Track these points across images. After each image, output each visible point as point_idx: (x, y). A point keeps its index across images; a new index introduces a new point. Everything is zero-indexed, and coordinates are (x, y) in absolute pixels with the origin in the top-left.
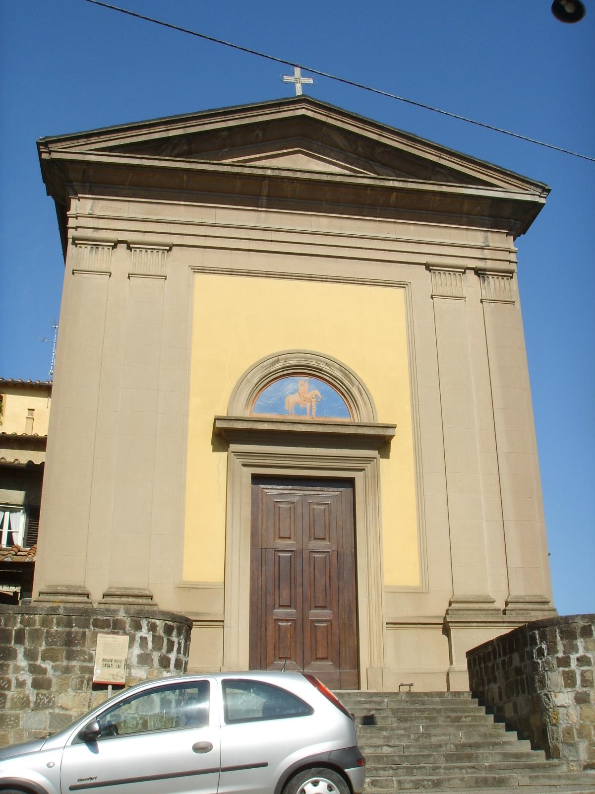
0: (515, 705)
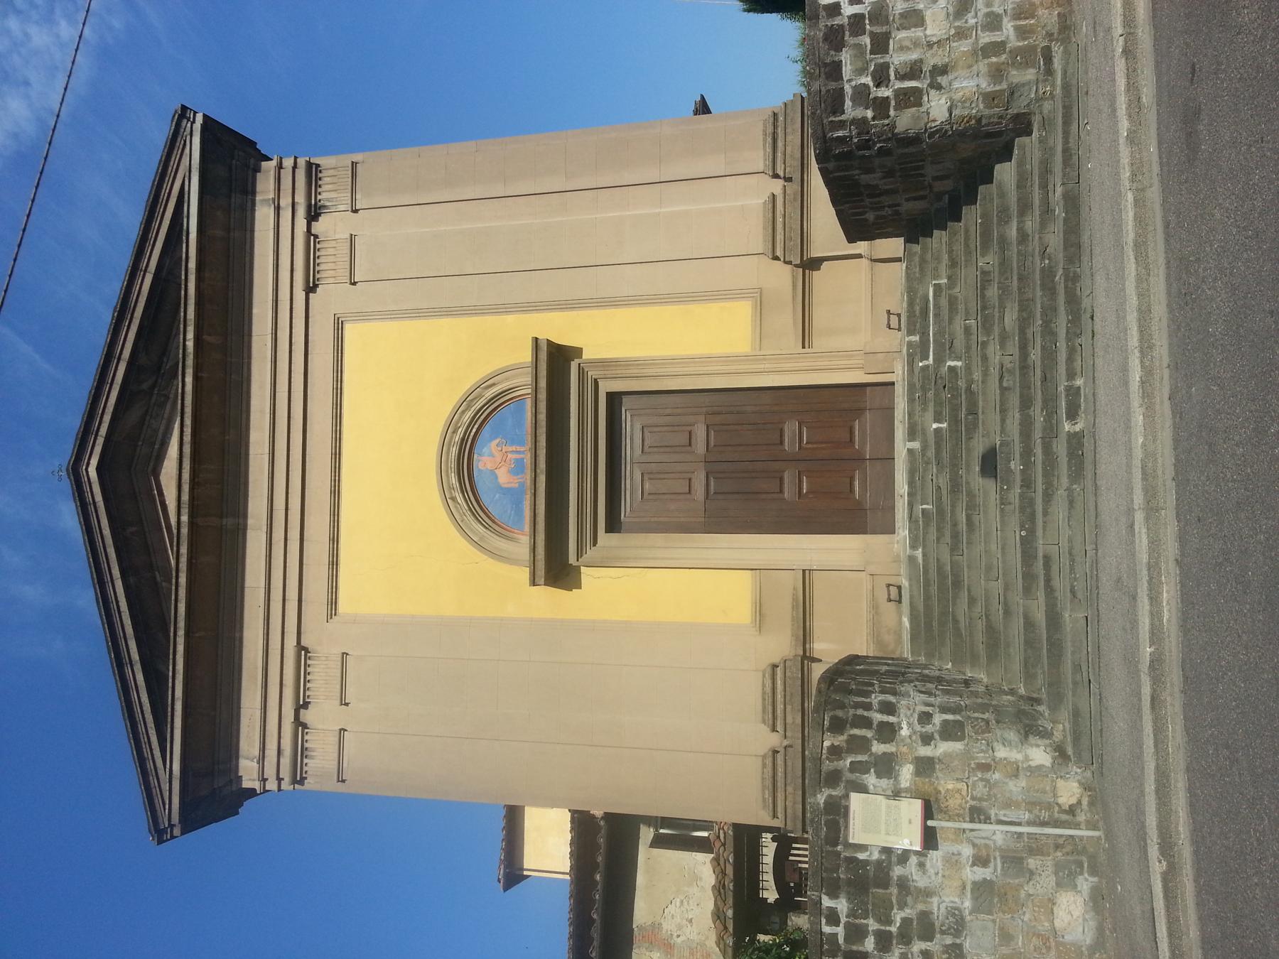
0: (936, 178)
